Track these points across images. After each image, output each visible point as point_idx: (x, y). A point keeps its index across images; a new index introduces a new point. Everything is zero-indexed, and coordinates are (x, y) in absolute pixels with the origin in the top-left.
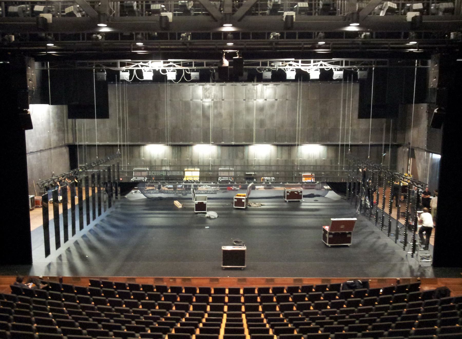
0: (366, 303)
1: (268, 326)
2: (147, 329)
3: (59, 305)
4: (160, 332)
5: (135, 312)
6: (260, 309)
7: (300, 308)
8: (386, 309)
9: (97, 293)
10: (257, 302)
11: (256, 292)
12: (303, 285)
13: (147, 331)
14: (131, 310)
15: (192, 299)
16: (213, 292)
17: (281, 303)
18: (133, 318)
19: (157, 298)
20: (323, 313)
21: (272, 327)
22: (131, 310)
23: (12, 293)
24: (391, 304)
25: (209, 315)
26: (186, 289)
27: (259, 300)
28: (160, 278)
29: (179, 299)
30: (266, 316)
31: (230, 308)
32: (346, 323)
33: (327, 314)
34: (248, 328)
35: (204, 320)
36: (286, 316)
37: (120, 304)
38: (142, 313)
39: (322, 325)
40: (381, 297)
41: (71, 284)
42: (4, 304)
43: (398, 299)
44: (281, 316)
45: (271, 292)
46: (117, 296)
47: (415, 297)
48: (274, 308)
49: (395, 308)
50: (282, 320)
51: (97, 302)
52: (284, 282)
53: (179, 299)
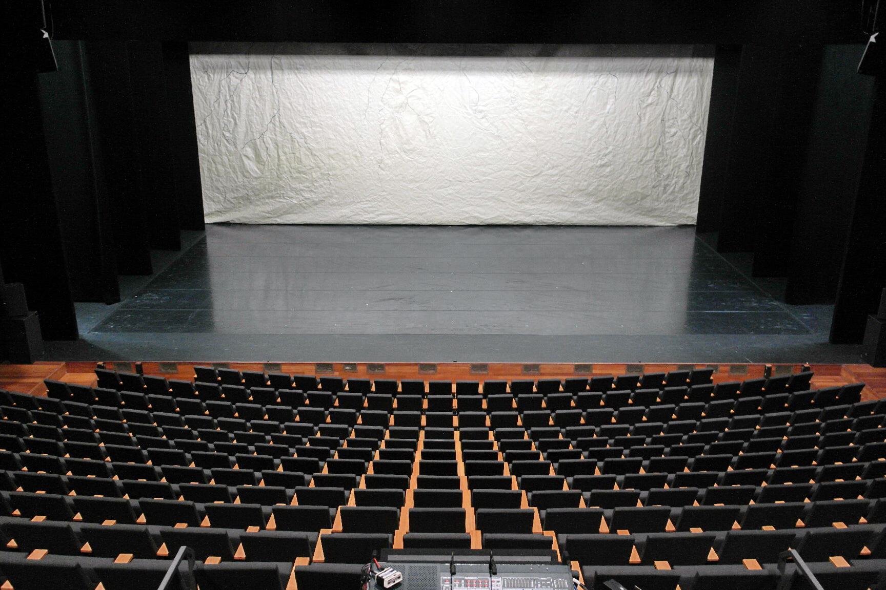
0: (684, 414)
1: (500, 458)
2: (332, 452)
3: (114, 415)
4: (660, 444)
5: (255, 427)
6: (488, 422)
7: (561, 421)
8: (721, 426)
9: (213, 394)
10: (481, 410)
11: (481, 389)
12: (595, 377)
13: (333, 456)
14: (249, 424)
15: (392, 403)
16: (427, 390)
17: (526, 412)
18: (251, 440)
19: (326, 402)
20: (603, 432)
21: (508, 458)
22: (249, 424)
23: (50, 395)
24: (731, 416)
25: (393, 434)
26: (350, 382)
27: (485, 405)
28: (171, 364)
29: (337, 403)
30: (498, 437)
31: (431, 421)
32: (646, 454)
33: (611, 433)
34: (464, 461)
35: (383, 446)
36: (534, 436)
37: (258, 414)
38: (268, 429)
39: (600, 456)
40: (713, 402)
41: (162, 378)
42: (12, 415)
43: (743, 408)
44: (526, 438)
45: (508, 390)
46: (251, 398)
47: (803, 402)
48: (512, 421)
49: (737, 424)
50: (528, 445)
51: (216, 411)
52: (556, 371)
53: (337, 403)
